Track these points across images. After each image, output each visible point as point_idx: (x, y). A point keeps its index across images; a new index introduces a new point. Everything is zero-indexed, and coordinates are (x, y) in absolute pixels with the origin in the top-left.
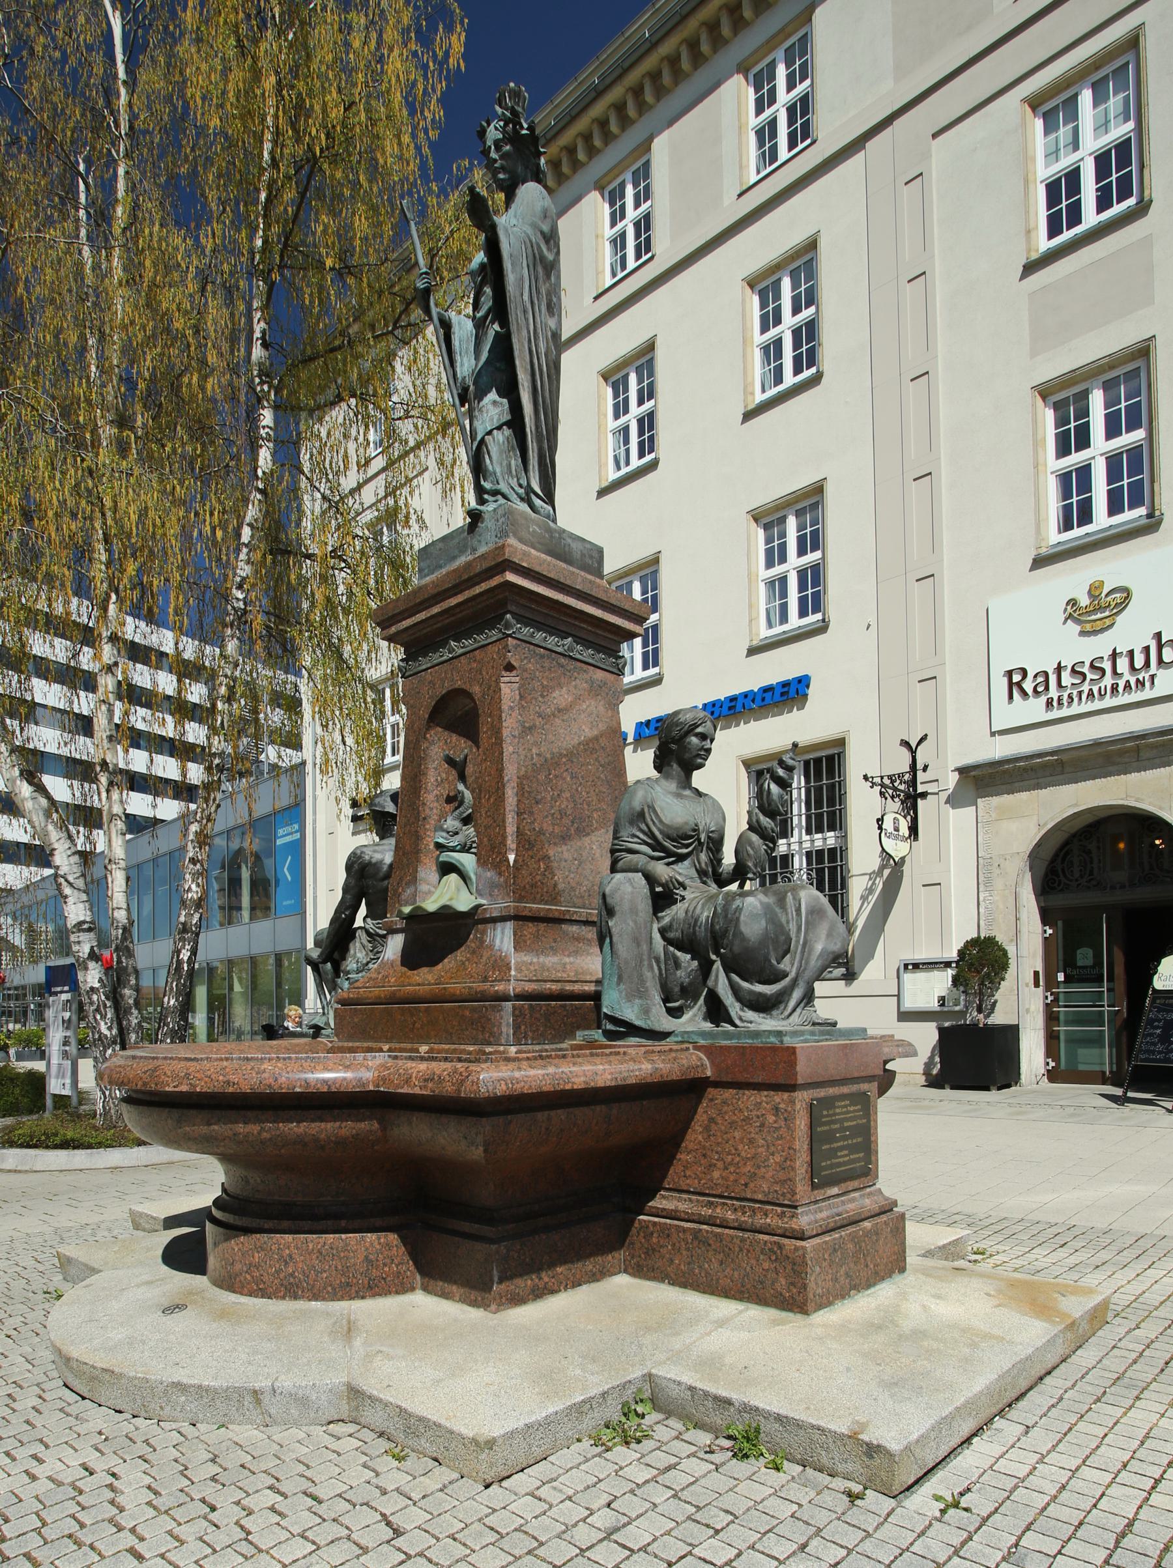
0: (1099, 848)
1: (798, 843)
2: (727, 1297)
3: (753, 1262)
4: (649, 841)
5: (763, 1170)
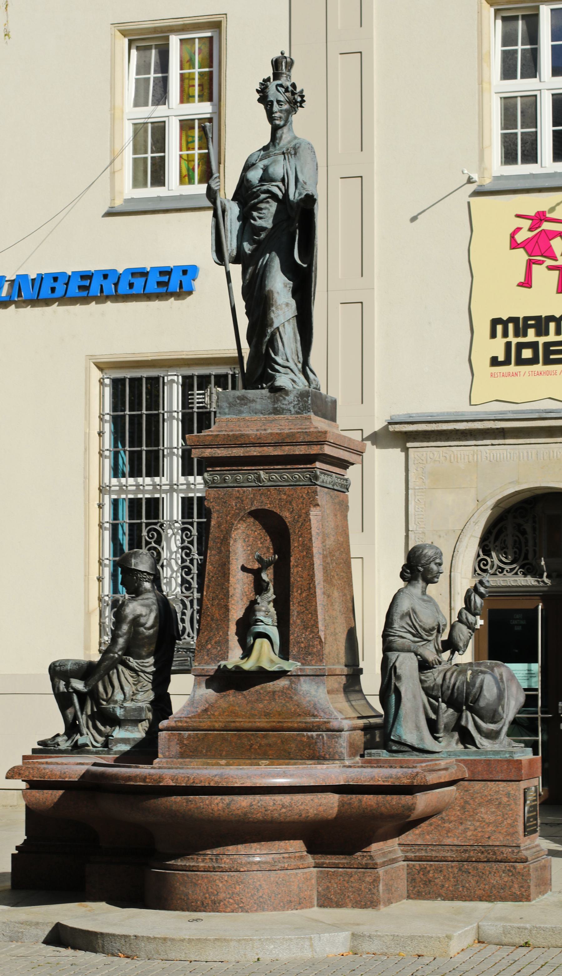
0: (534, 529)
1: (174, 485)
2: (481, 900)
3: (498, 878)
4: (413, 631)
5: (500, 828)
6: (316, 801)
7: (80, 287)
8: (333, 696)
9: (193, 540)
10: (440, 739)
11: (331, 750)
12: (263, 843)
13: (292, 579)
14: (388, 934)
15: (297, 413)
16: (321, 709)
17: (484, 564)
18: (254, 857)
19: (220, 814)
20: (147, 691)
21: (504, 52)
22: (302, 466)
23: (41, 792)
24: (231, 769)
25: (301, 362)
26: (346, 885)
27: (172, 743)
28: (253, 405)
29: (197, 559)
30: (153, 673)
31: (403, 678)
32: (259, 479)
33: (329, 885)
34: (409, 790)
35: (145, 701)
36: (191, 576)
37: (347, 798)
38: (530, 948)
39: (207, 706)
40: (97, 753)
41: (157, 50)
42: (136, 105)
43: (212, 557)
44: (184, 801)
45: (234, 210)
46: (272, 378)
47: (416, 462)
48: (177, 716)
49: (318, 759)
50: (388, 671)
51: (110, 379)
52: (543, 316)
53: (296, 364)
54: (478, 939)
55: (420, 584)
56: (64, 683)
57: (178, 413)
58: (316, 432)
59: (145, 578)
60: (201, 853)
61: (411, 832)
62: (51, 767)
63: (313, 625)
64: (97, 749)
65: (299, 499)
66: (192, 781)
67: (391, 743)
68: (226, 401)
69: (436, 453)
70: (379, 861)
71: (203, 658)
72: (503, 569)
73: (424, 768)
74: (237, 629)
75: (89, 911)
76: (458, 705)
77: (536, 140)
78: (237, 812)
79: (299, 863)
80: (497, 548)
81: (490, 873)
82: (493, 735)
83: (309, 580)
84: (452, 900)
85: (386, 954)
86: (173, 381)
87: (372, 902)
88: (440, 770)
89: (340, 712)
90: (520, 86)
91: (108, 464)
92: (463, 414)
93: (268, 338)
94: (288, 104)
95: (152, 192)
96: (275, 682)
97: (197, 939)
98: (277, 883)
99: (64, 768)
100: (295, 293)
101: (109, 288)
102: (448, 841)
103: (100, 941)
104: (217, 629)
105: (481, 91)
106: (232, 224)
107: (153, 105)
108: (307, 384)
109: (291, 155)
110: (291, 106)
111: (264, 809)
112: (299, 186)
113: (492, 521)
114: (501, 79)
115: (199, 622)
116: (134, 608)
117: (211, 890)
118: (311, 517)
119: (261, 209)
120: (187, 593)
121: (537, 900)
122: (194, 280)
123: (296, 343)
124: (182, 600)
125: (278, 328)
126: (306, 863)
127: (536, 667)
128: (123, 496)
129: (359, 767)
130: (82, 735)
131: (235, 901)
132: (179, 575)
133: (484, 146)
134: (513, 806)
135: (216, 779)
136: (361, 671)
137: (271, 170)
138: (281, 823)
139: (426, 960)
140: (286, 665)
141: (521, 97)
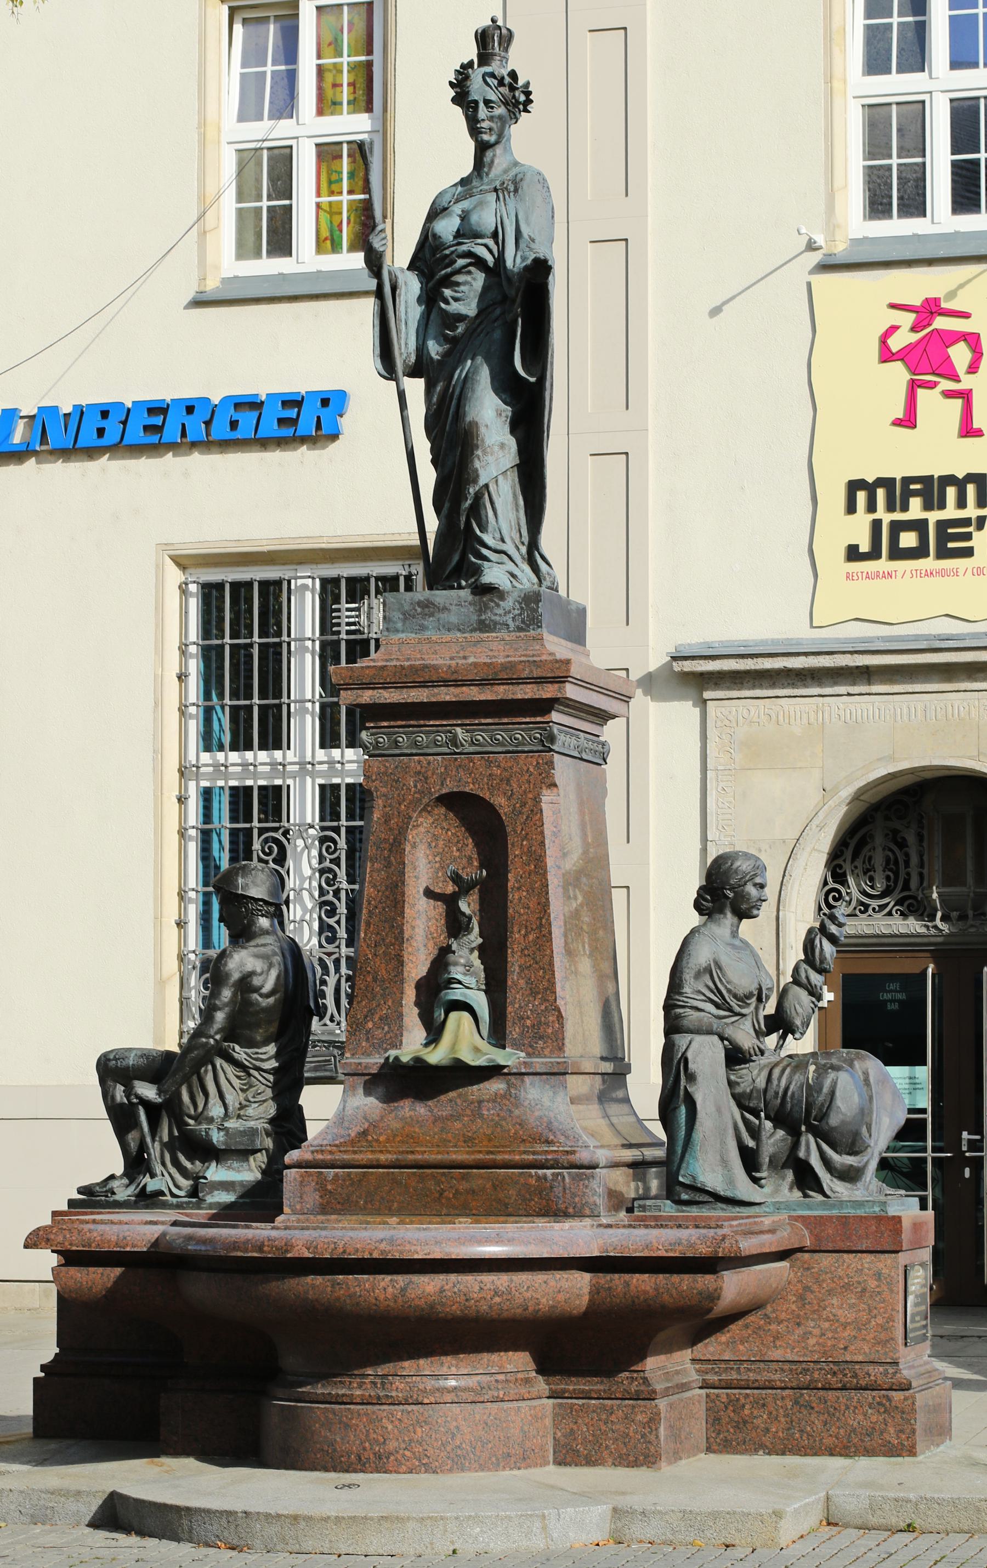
0: (920, 838)
1: (308, 765)
2: (832, 1455)
3: (861, 1417)
6: (552, 1283)
7: (146, 428)
8: (581, 1107)
9: (339, 858)
10: (763, 1181)
11: (577, 1199)
12: (461, 1356)
13: (511, 911)
14: (676, 1509)
15: (520, 629)
16: (560, 1130)
17: (834, 897)
18: (447, 1379)
19: (388, 1306)
20: (264, 1101)
21: (868, 28)
22: (528, 720)
23: (84, 1270)
24: (407, 1229)
25: (526, 543)
26: (604, 1428)
27: (307, 1189)
28: (443, 616)
29: (347, 890)
30: (274, 1071)
31: (699, 1079)
32: (454, 741)
33: (575, 1427)
34: (709, 1265)
35: (260, 1118)
36: (336, 918)
37: (604, 1279)
38: (915, 1534)
39: (366, 1125)
40: (179, 1206)
41: (278, 25)
42: (242, 118)
43: (375, 874)
44: (328, 1283)
45: (411, 286)
46: (478, 571)
47: (719, 724)
48: (315, 1143)
49: (556, 1215)
50: (675, 1067)
51: (198, 583)
52: (936, 477)
53: (518, 549)
54: (828, 1519)
55: (729, 918)
56: (123, 1088)
57: (313, 641)
58: (551, 661)
59: (260, 910)
60: (356, 1372)
61: (713, 1338)
62: (100, 1227)
63: (546, 989)
64: (179, 1200)
65: (522, 775)
66: (341, 1250)
67: (678, 1188)
68: (399, 609)
69: (753, 710)
70: (659, 1387)
71: (359, 1044)
72: (866, 906)
73: (735, 1229)
74: (418, 996)
75: (167, 1472)
76: (793, 1126)
77: (924, 179)
78: (417, 1302)
79: (523, 1391)
80: (856, 871)
81: (847, 1408)
82: (852, 1174)
83: (540, 913)
84: (783, 1454)
85: (670, 1543)
86: (305, 587)
87: (647, 1456)
88: (762, 1232)
89: (593, 1136)
90: (896, 85)
91: (194, 727)
92: (799, 642)
93: (469, 502)
94: (503, 107)
95: (270, 266)
96: (481, 1085)
97: (350, 1518)
98: (487, 1424)
99: (124, 1230)
100: (516, 426)
101: (196, 430)
102: (777, 1354)
103: (185, 1522)
104: (384, 996)
105: (830, 95)
106: (409, 310)
107: (270, 119)
108: (535, 580)
109: (509, 193)
110: (509, 111)
111: (463, 1298)
112: (522, 245)
113: (847, 826)
114: (864, 75)
115: (351, 998)
116: (243, 961)
117: (373, 1436)
118: (544, 806)
119: (458, 284)
120: (330, 948)
121: (928, 1454)
122: (341, 416)
123: (517, 510)
124: (320, 959)
125: (487, 486)
126: (534, 1391)
127: (923, 1073)
128: (221, 783)
129: (624, 1226)
130: (153, 1176)
131: (414, 1453)
132: (315, 916)
133: (835, 186)
134: (886, 1294)
135: (383, 1246)
136: (627, 1069)
137: (474, 218)
138: (493, 1321)
139: (738, 1553)
140: (504, 1057)
141: (898, 104)
